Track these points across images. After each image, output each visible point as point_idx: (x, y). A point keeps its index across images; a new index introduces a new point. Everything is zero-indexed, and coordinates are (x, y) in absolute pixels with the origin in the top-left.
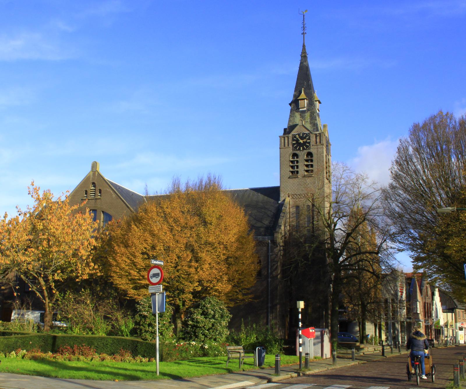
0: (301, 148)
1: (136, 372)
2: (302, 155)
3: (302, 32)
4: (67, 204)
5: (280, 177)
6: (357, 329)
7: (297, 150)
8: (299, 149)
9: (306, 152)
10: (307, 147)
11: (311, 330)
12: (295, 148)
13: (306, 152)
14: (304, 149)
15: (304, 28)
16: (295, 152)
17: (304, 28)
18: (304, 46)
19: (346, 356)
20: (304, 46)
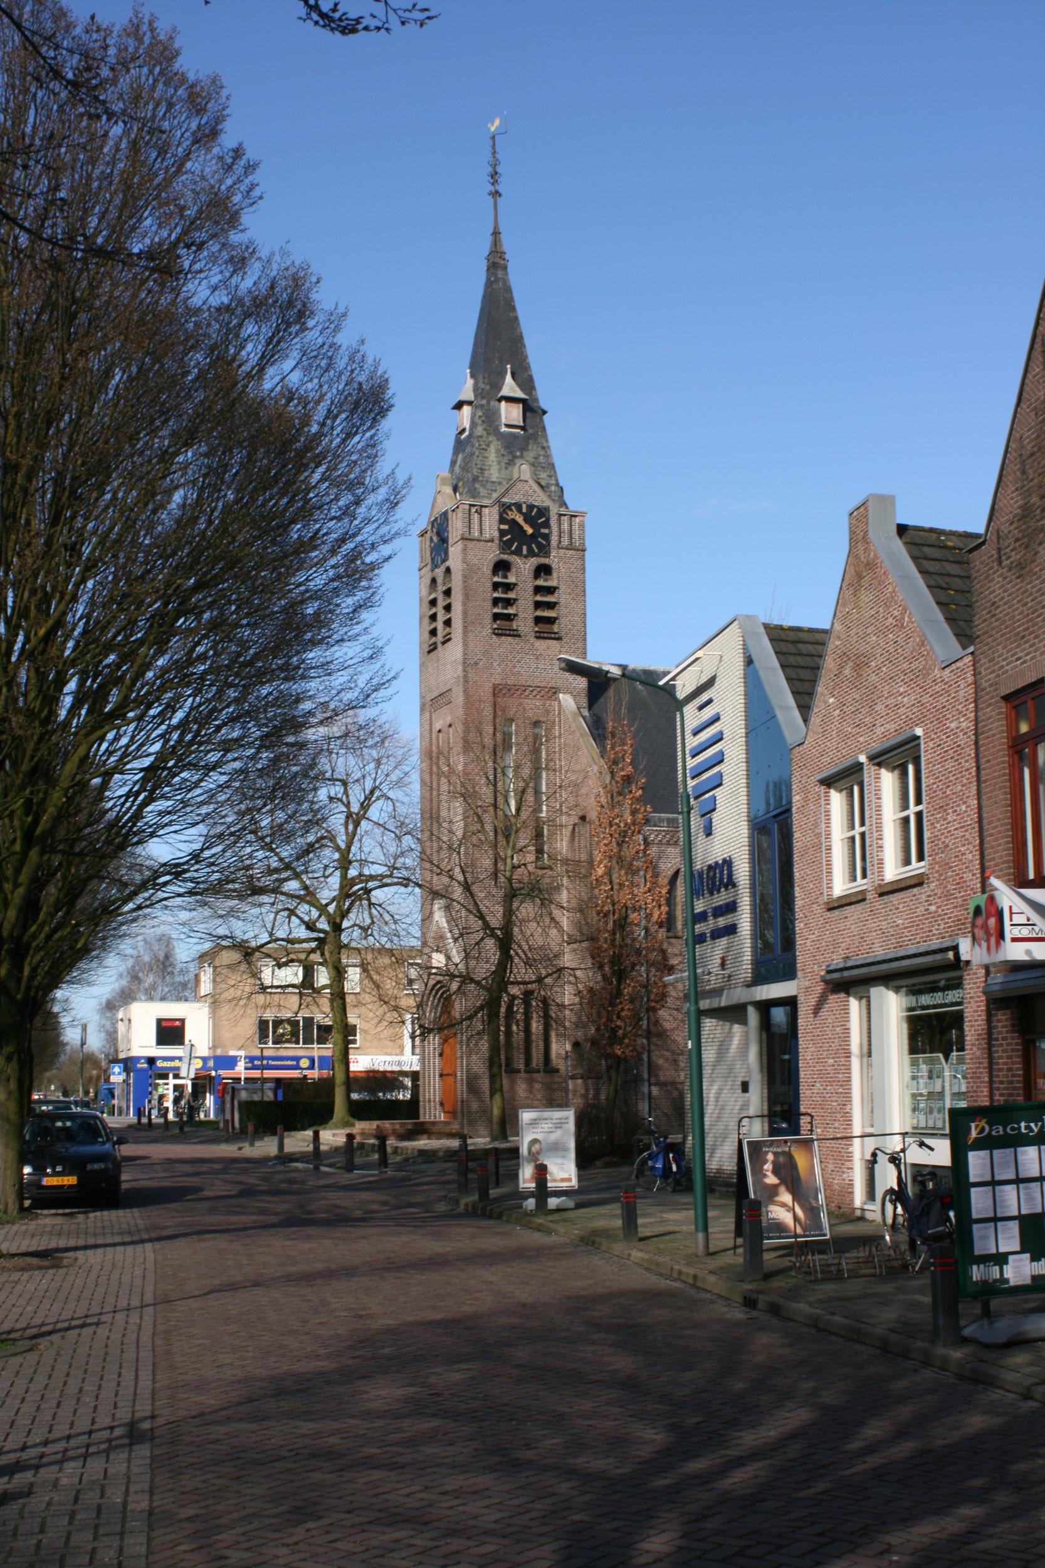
0: (525, 548)
1: (40, 1281)
2: (523, 568)
3: (492, 188)
4: (139, 661)
5: (585, 640)
6: (44, 1108)
7: (513, 553)
8: (518, 552)
9: (534, 562)
10: (541, 547)
11: (314, 1074)
12: (505, 546)
13: (534, 562)
14: (531, 554)
15: (494, 176)
16: (505, 557)
17: (494, 176)
18: (496, 233)
19: (188, 1168)
20: (496, 233)
